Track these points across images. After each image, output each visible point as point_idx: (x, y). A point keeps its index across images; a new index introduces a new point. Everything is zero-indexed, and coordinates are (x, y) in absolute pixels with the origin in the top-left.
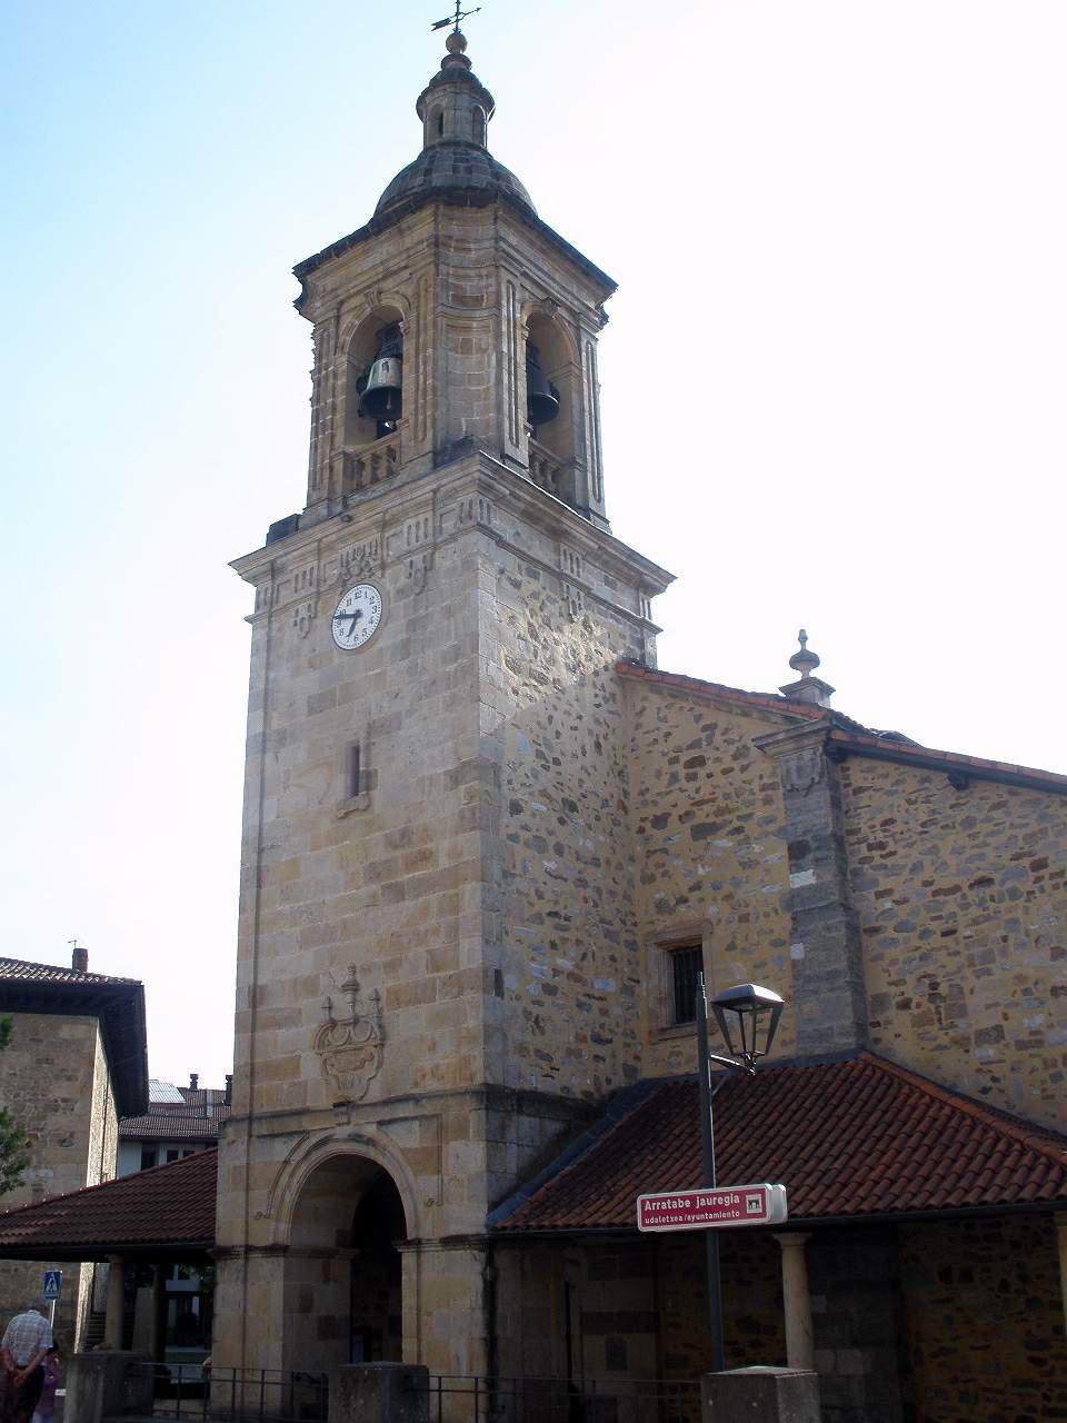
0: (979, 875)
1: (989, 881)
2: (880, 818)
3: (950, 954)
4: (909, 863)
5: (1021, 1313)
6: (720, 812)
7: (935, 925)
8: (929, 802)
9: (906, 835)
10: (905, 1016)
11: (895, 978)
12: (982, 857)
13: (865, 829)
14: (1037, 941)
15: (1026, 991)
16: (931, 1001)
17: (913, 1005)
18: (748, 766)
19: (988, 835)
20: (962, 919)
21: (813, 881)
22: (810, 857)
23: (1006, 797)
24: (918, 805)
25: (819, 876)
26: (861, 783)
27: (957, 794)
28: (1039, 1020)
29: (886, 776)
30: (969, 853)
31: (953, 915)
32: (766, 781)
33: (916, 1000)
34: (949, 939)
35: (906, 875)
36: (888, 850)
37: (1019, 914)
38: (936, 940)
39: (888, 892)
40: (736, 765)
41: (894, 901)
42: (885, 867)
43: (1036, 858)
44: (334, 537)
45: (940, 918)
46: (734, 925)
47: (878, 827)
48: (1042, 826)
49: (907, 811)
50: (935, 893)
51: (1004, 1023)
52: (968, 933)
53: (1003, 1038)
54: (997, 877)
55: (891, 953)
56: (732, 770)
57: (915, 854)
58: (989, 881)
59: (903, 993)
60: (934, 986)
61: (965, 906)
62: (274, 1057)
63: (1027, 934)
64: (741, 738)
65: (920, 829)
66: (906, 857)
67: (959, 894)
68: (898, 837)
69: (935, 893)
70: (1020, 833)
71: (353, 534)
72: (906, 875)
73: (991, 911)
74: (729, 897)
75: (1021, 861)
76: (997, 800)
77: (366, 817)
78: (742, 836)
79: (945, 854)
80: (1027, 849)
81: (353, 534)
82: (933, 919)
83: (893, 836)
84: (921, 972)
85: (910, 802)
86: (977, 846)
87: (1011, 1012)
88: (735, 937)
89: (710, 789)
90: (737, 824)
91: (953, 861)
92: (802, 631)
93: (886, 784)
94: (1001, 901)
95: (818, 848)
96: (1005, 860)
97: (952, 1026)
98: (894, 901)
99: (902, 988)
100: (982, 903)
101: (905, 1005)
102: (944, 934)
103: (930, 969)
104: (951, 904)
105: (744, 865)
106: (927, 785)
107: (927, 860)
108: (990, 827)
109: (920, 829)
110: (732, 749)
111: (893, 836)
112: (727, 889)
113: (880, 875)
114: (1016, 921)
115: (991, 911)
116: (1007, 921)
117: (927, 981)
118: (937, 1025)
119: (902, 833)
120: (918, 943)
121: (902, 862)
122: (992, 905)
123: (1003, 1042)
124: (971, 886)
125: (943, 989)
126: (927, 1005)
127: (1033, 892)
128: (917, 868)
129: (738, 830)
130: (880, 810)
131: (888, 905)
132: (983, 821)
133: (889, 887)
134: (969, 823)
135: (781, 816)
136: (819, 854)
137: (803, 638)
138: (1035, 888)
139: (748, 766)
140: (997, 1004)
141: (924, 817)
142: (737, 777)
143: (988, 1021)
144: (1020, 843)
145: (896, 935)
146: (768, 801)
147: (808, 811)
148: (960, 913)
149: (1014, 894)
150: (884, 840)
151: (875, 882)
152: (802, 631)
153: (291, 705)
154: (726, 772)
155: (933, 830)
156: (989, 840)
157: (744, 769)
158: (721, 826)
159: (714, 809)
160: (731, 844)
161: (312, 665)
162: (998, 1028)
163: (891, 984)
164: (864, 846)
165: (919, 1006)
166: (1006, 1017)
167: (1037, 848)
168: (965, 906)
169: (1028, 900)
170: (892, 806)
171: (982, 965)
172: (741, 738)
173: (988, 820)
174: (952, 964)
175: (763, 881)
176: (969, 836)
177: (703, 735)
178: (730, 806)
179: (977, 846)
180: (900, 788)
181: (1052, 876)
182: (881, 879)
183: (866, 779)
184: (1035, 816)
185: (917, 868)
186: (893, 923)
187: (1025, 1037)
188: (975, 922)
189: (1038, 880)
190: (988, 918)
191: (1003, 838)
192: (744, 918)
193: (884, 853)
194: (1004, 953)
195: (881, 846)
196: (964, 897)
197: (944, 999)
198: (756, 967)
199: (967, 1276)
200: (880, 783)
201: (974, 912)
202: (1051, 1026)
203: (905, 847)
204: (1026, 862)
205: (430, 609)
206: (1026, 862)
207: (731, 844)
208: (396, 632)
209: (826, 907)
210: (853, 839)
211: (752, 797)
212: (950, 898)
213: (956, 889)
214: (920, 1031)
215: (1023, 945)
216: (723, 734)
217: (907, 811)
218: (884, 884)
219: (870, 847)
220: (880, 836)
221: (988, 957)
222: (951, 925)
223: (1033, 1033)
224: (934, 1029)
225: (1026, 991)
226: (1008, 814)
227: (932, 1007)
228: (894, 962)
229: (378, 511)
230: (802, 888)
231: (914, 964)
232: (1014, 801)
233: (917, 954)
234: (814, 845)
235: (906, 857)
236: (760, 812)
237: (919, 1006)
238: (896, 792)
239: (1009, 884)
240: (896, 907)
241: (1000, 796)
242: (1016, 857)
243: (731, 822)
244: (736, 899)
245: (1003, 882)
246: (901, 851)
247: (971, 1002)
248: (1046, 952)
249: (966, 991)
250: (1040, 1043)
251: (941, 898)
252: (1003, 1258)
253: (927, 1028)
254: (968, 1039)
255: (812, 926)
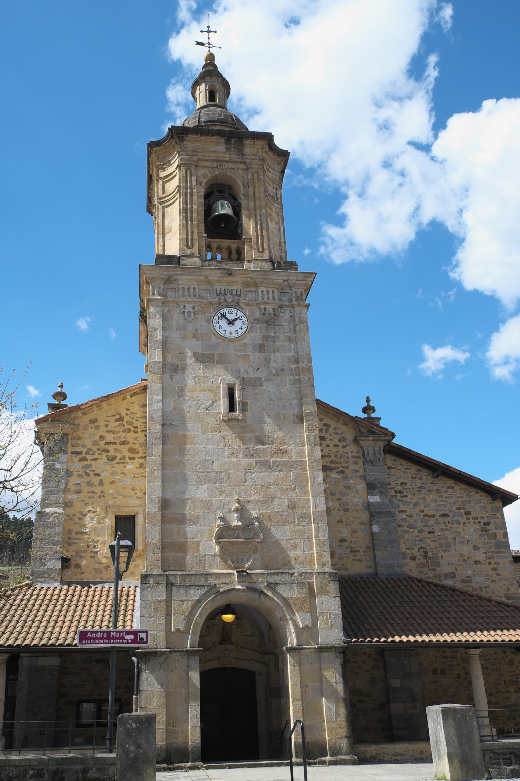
0: (443, 512)
1: (448, 516)
2: (399, 481)
3: (432, 541)
4: (414, 501)
5: (466, 687)
6: (332, 462)
7: (425, 528)
8: (421, 479)
9: (411, 490)
10: (413, 563)
11: (408, 546)
12: (445, 506)
13: (393, 484)
14: (468, 542)
15: (464, 561)
16: (424, 558)
17: (417, 559)
18: (346, 446)
19: (446, 498)
20: (436, 529)
21: (379, 500)
22: (377, 490)
23: (453, 485)
24: (417, 479)
25: (381, 499)
26: (391, 465)
27: (433, 479)
28: (470, 572)
29: (402, 465)
30: (439, 503)
31: (433, 526)
32: (354, 454)
33: (418, 557)
34: (432, 535)
35: (411, 506)
36: (404, 495)
37: (460, 530)
38: (426, 535)
39: (404, 511)
40: (341, 444)
41: (407, 515)
42: (403, 501)
43: (466, 510)
44: (216, 278)
45: (427, 526)
46: (342, 512)
47: (399, 484)
48: (469, 499)
49: (412, 481)
50: (425, 516)
51: (455, 571)
52: (439, 534)
53: (455, 577)
54: (451, 515)
55: (407, 536)
56: (338, 446)
57: (415, 499)
58: (448, 516)
59: (412, 553)
60: (426, 553)
61: (438, 523)
62: (178, 540)
63: (463, 538)
64: (342, 434)
65: (418, 489)
66: (411, 499)
67: (435, 518)
68: (408, 490)
69: (425, 516)
70: (460, 500)
71: (228, 282)
72: (411, 506)
73: (449, 527)
74: (339, 499)
75: (460, 510)
76: (450, 485)
77: (243, 424)
78: (344, 475)
79: (428, 501)
80: (462, 506)
81: (228, 282)
82: (424, 526)
83: (406, 489)
84: (420, 546)
85: (412, 477)
86: (442, 501)
87: (458, 568)
88: (341, 517)
89: (328, 452)
90: (341, 469)
91: (432, 505)
92: (368, 397)
93: (403, 468)
94: (453, 524)
95: (381, 487)
96: (454, 508)
97: (434, 569)
98: (407, 515)
99: (412, 551)
100: (444, 523)
101: (413, 558)
102: (429, 533)
103: (424, 546)
104: (431, 521)
105: (346, 487)
106: (420, 472)
107: (421, 502)
108: (447, 494)
109: (418, 489)
110: (338, 437)
111: (406, 489)
112: (338, 496)
113: (401, 504)
114: (459, 533)
115: (449, 527)
116: (455, 532)
117: (423, 550)
118: (427, 569)
119: (409, 489)
120: (418, 534)
121: (410, 500)
122: (449, 525)
123: (455, 579)
124: (440, 516)
125: (430, 554)
126: (422, 560)
127: (466, 523)
128: (416, 504)
129: (342, 472)
130: (400, 478)
131: (404, 517)
132: (444, 492)
133: (404, 509)
134: (438, 491)
135: (362, 470)
136: (381, 490)
137: (368, 400)
138: (467, 521)
139: (346, 446)
140: (453, 564)
141: (419, 485)
142: (340, 449)
143: (449, 570)
144: (460, 504)
145: (408, 529)
146: (355, 463)
147: (376, 471)
148: (435, 526)
149: (458, 522)
150: (402, 490)
151: (399, 506)
152: (368, 397)
153: (181, 353)
154: (335, 446)
155: (424, 491)
156: (447, 500)
157: (344, 447)
158: (334, 468)
159: (330, 460)
160: (339, 477)
161: (195, 337)
162: (453, 573)
163: (407, 549)
164: (393, 491)
165: (419, 559)
166: (456, 569)
167: (466, 507)
168: (438, 523)
169: (464, 526)
170: (405, 477)
171: (446, 547)
172: (342, 434)
173: (446, 492)
174: (433, 545)
175: (355, 496)
176: (439, 496)
177: (324, 428)
178: (337, 461)
179: (442, 501)
180: (408, 471)
181: (473, 519)
182: (401, 505)
183: (393, 464)
184: (465, 494)
185: (416, 504)
186: (407, 524)
187: (464, 578)
188: (442, 530)
189: (468, 519)
190: (447, 530)
191: (453, 500)
192: (346, 510)
193: (402, 495)
194: (455, 544)
195: (400, 492)
196: (437, 519)
197: (430, 558)
198: (353, 532)
199: (443, 672)
200: (399, 467)
201: (442, 526)
202: (474, 575)
203: (411, 495)
204: (463, 511)
205: (277, 334)
206: (463, 511)
207: (339, 477)
208: (257, 336)
209: (386, 512)
210: (389, 487)
211: (347, 460)
212: (432, 519)
213: (433, 516)
214: (420, 569)
215: (462, 542)
216: (333, 430)
217: (412, 481)
218: (402, 508)
219: (396, 492)
220: (400, 488)
221: (448, 545)
222: (431, 529)
223: (467, 577)
224: (426, 570)
225: (464, 561)
226: (454, 491)
227: (425, 561)
228: (408, 540)
229: (247, 276)
230: (374, 502)
231: (417, 542)
232: (456, 487)
233: (418, 539)
234: (379, 486)
235: (411, 499)
236: (352, 467)
237: (419, 559)
238: (406, 472)
239: (456, 518)
240: (408, 518)
241: (451, 484)
242: (458, 509)
243: (338, 468)
244: (342, 501)
245: (453, 517)
246: (410, 496)
247: (442, 561)
248: (471, 547)
249: (440, 556)
250: (470, 581)
251: (427, 518)
252: (458, 665)
253: (424, 569)
254: (441, 576)
255: (381, 519)
